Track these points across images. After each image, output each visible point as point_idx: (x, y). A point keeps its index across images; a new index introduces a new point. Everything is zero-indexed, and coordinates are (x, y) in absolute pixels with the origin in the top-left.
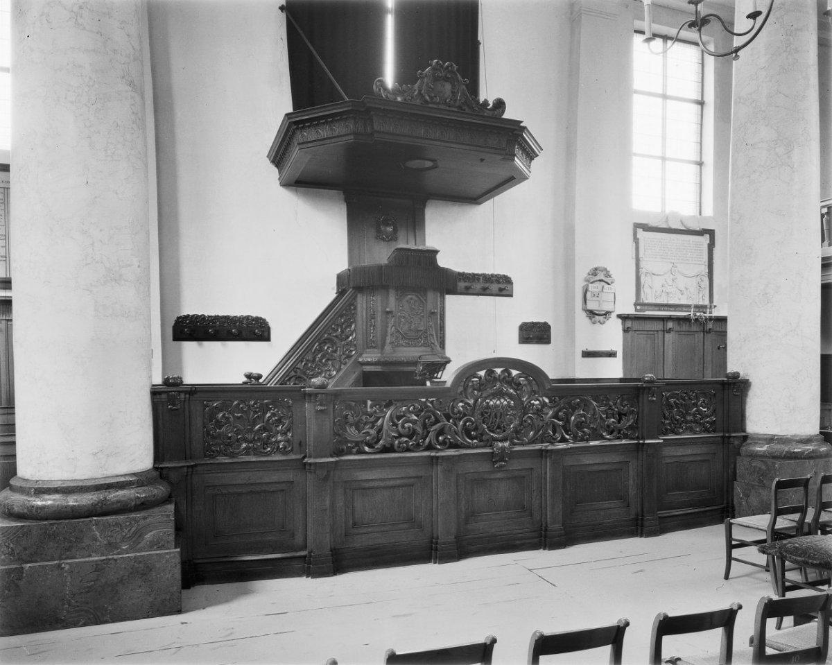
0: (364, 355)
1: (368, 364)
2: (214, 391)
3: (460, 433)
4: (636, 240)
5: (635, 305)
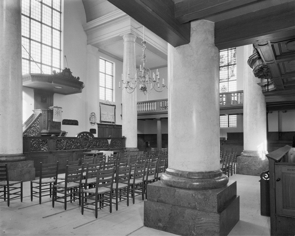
0: (42, 131)
1: (44, 133)
4: (100, 106)
5: (100, 121)
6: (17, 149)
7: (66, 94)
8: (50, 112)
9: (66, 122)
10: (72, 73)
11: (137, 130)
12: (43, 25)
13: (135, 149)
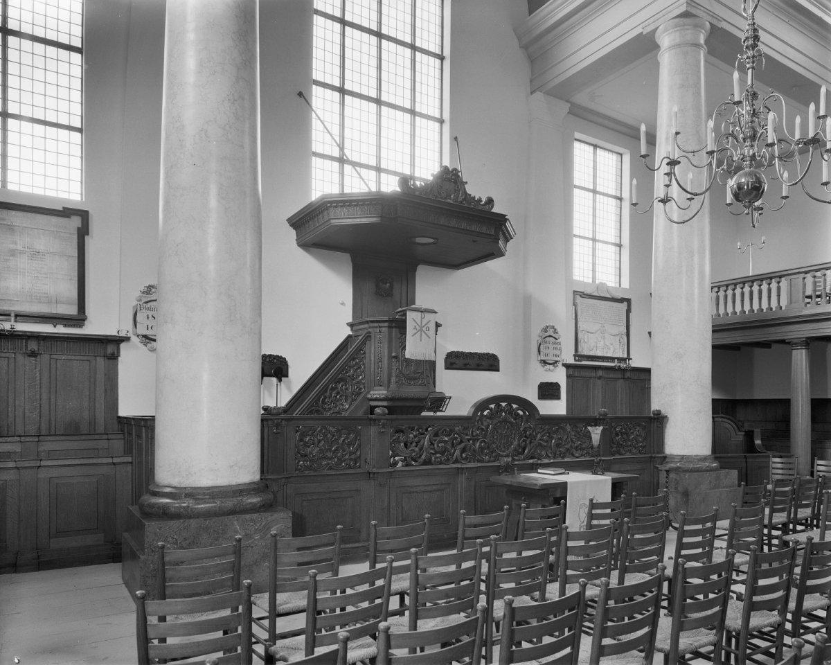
0: (372, 392)
1: (376, 399)
2: (449, 419)
3: (532, 446)
4: (575, 305)
5: (575, 356)
6: (231, 467)
7: (457, 266)
8: (396, 327)
9: (483, 363)
10: (466, 183)
11: (710, 385)
12: (383, 41)
13: (704, 459)
